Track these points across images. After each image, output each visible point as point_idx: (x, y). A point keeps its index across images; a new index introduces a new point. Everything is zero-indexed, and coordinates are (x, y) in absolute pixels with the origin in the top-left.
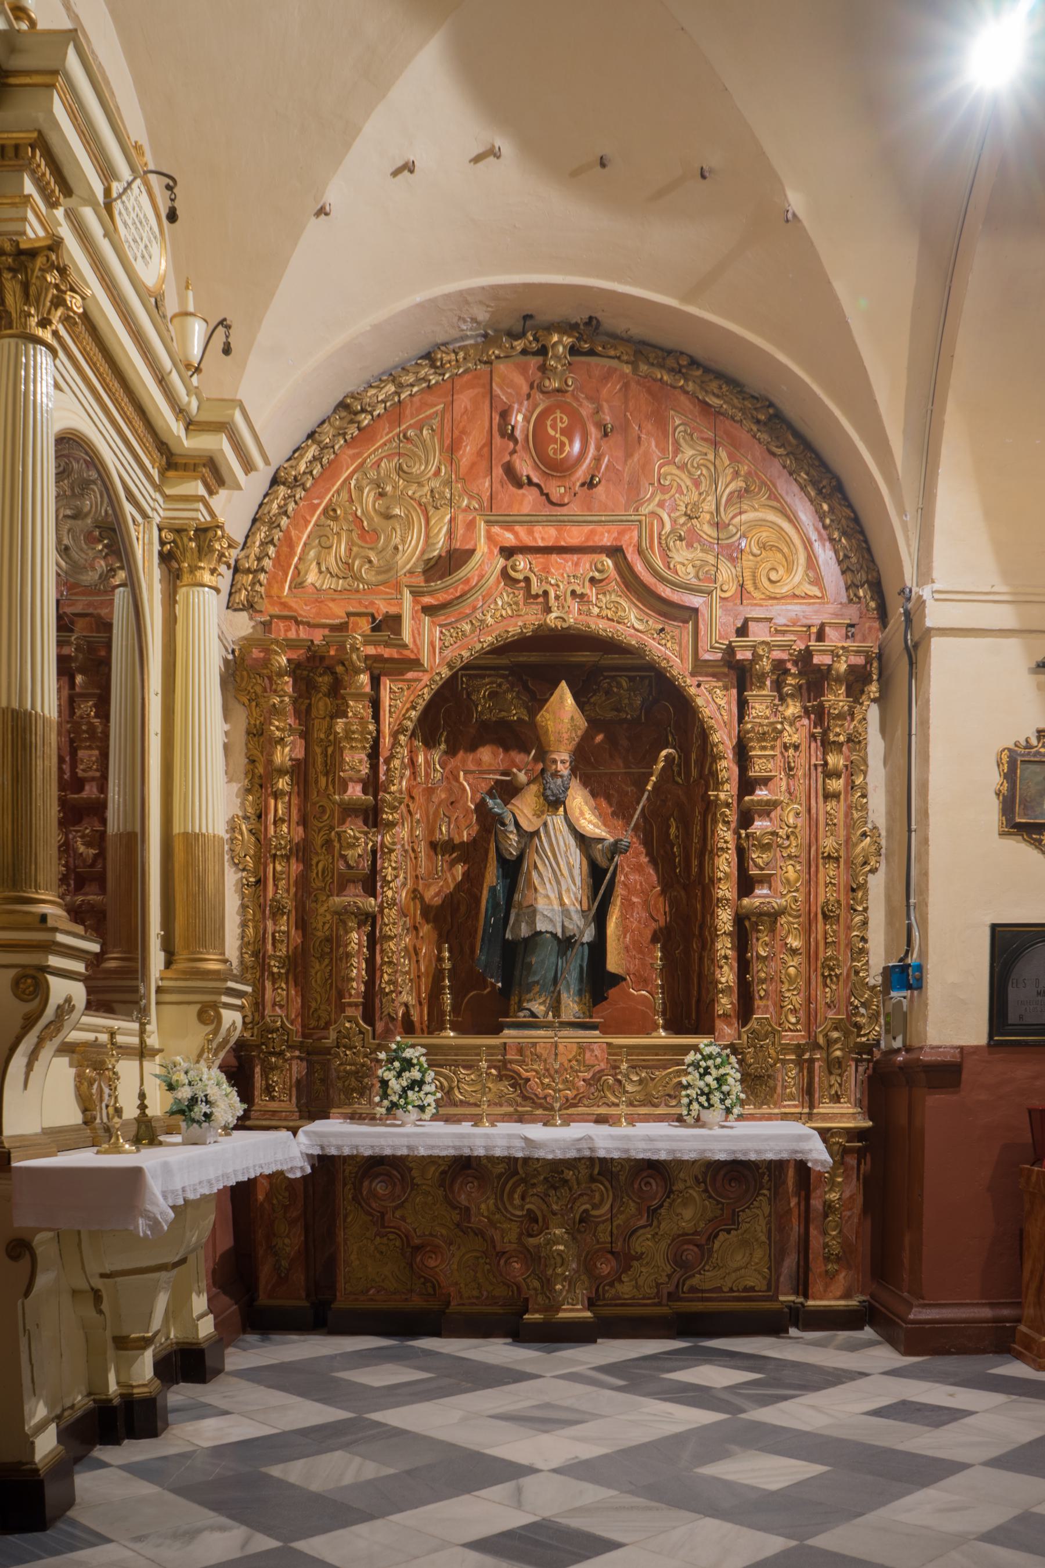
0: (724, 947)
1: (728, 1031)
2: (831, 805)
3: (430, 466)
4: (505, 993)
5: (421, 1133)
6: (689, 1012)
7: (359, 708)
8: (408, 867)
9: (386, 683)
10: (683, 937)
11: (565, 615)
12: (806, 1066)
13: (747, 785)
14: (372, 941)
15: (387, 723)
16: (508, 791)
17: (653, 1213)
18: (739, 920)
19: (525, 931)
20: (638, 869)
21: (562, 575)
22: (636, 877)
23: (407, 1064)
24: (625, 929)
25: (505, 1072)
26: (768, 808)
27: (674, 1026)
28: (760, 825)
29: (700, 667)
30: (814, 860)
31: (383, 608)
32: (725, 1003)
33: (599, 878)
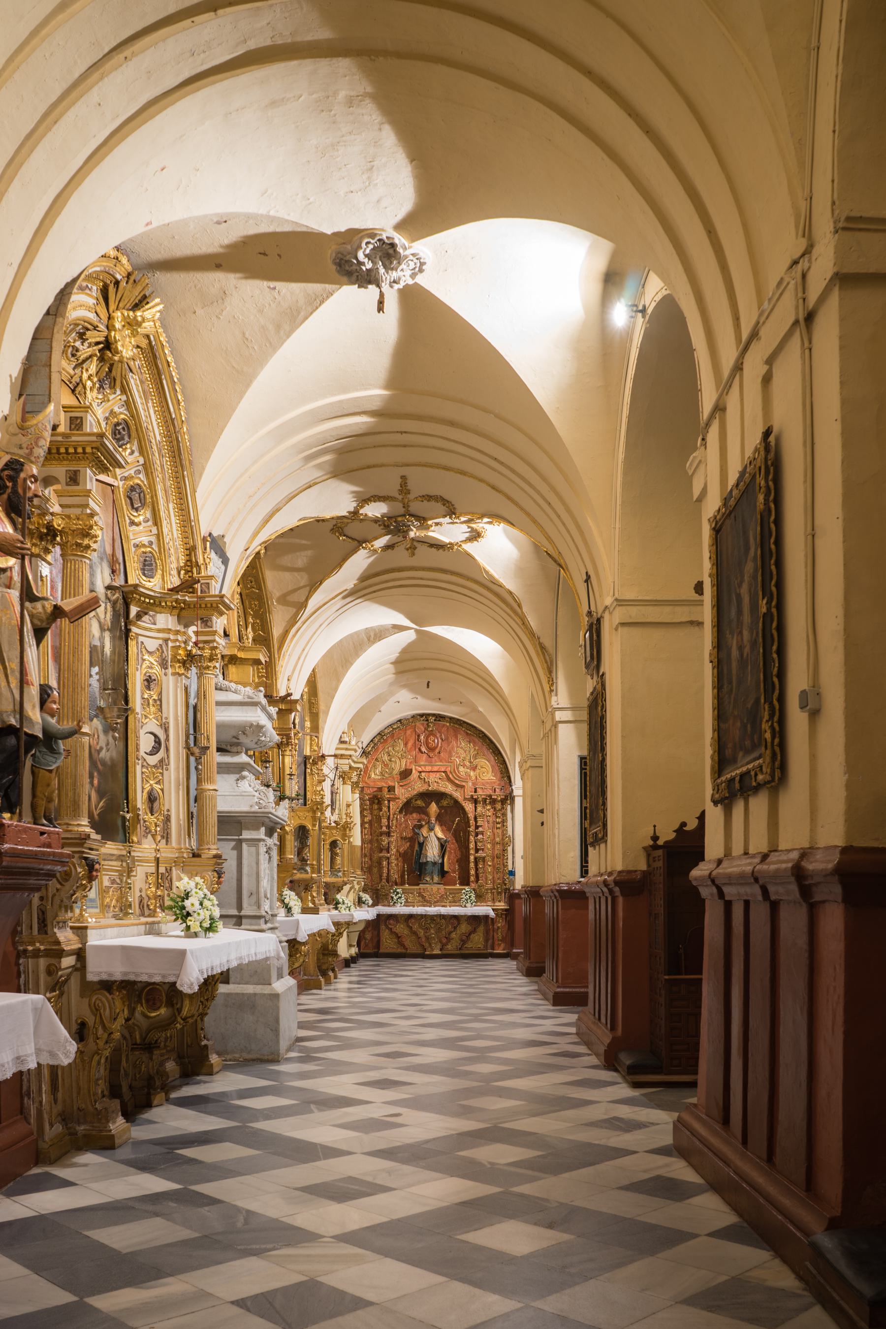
0: (472, 865)
1: (473, 885)
2: (498, 831)
3: (400, 745)
4: (420, 875)
5: (400, 909)
6: (465, 881)
7: (385, 809)
8: (395, 844)
9: (391, 803)
10: (463, 861)
11: (433, 787)
12: (492, 893)
13: (477, 827)
14: (388, 864)
15: (392, 812)
16: (421, 826)
17: (455, 928)
18: (476, 858)
19: (425, 861)
20: (453, 843)
21: (432, 778)
22: (452, 846)
23: (398, 893)
24: (449, 859)
25: (420, 895)
26: (482, 833)
27: (461, 884)
28: (480, 836)
29: (465, 799)
30: (494, 844)
31: (391, 784)
32: (472, 878)
33: (443, 846)
